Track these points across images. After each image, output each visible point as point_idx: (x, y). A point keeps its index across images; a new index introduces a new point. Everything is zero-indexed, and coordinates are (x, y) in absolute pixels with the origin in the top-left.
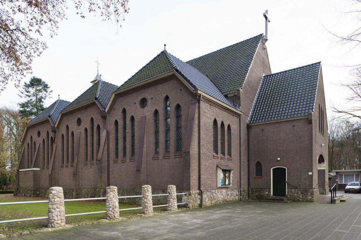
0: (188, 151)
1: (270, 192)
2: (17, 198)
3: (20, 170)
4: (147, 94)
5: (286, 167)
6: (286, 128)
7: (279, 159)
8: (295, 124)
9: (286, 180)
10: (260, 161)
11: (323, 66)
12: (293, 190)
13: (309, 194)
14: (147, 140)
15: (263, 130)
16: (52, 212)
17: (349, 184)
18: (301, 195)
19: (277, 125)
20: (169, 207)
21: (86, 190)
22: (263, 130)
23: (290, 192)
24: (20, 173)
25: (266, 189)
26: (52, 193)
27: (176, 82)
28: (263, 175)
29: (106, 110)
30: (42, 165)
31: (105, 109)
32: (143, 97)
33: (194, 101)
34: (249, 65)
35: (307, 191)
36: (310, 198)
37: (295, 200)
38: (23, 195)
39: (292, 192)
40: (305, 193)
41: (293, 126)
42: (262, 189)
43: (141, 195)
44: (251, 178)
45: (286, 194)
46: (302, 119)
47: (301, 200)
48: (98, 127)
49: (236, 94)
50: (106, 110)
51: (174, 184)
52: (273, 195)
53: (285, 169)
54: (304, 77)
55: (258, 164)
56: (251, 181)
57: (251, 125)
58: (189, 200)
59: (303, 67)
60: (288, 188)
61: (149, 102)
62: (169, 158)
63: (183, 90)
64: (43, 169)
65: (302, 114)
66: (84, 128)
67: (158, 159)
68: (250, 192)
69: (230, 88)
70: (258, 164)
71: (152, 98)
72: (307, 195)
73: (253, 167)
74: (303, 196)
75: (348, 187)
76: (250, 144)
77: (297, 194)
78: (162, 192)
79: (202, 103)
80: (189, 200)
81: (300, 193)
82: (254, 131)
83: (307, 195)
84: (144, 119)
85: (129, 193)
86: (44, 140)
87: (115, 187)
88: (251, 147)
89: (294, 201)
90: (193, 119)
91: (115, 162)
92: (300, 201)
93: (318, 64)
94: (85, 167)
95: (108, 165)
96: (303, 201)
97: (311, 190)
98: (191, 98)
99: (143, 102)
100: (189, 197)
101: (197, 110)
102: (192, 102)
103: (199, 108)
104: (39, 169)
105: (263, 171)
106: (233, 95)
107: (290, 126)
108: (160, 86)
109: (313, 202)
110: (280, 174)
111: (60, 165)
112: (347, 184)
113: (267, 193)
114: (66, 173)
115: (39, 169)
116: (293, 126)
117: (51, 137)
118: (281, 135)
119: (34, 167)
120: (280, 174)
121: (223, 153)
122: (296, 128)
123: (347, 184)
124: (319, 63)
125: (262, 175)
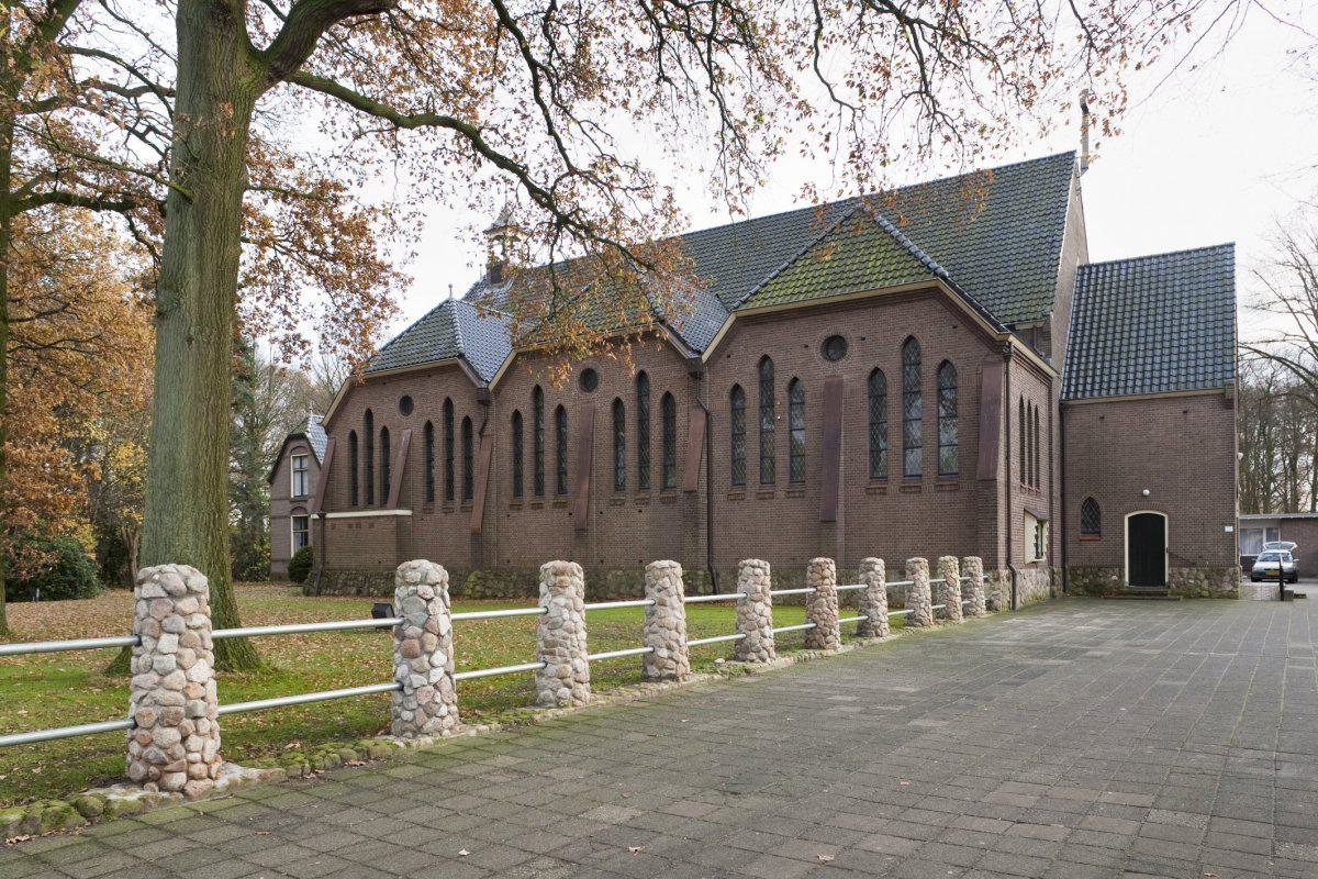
0: (991, 477)
1: (1121, 576)
2: (325, 604)
3: (329, 515)
4: (844, 326)
5: (1165, 512)
6: (1167, 415)
7: (1147, 492)
8: (1190, 405)
9: (1167, 546)
10: (1095, 496)
11: (1240, 256)
12: (1185, 571)
13: (1227, 578)
14: (847, 443)
15: (1102, 418)
16: (877, 607)
17: (1260, 556)
18: (1206, 582)
19: (1141, 408)
20: (972, 607)
21: (620, 573)
22: (1102, 418)
23: (1177, 576)
24: (328, 524)
25: (1112, 567)
26: (873, 570)
27: (939, 307)
28: (1103, 531)
29: (705, 357)
30: (420, 500)
31: (700, 353)
32: (832, 333)
33: (996, 358)
34: (1056, 244)
35: (1221, 573)
36: (1230, 588)
37: (1192, 595)
38: (354, 590)
39: (1181, 574)
40: (1216, 577)
41: (1185, 412)
42: (1099, 568)
43: (643, 597)
44: (1069, 539)
45: (1167, 580)
46: (1208, 395)
47: (1205, 593)
48: (668, 398)
49: (1040, 325)
50: (705, 357)
51: (923, 556)
52: (1131, 583)
53: (1163, 518)
54: (1195, 280)
55: (1091, 507)
56: (1070, 547)
57: (1071, 403)
58: (995, 592)
59: (1188, 252)
60: (1170, 565)
61: (854, 349)
62: (920, 492)
63: (961, 327)
64: (428, 511)
65: (1209, 384)
66: (611, 400)
67: (885, 494)
68: (1069, 577)
69: (1018, 305)
70: (1091, 507)
71: (864, 339)
72: (1222, 582)
73: (1075, 510)
74: (1210, 584)
75: (1259, 566)
76: (1068, 452)
77: (1196, 578)
78: (898, 576)
79: (1012, 364)
80: (995, 592)
81: (1202, 576)
82: (1077, 420)
83: (1222, 582)
84: (833, 391)
85: (788, 579)
86: (429, 427)
87: (574, 566)
88: (1068, 459)
89: (1188, 597)
90: (997, 401)
91: (732, 498)
92: (1204, 597)
93: (1229, 250)
94: (614, 510)
95: (710, 507)
96: (1210, 597)
97: (1231, 569)
98: (985, 350)
99: (835, 346)
100: (996, 584)
101: (1003, 379)
102: (989, 359)
103: (1007, 373)
104: (408, 512)
105: (1103, 523)
106: (1030, 326)
107: (1177, 410)
108: (889, 310)
109: (1236, 598)
110: (1147, 532)
111: (506, 501)
112: (1256, 557)
113: (1115, 577)
114: (452, 525)
115: (408, 512)
116: (1185, 412)
117: (462, 417)
118: (1152, 432)
119: (399, 506)
120: (1147, 532)
121: (1030, 483)
122: (1191, 416)
123: (1256, 557)
124: (1231, 245)
125: (1099, 533)
